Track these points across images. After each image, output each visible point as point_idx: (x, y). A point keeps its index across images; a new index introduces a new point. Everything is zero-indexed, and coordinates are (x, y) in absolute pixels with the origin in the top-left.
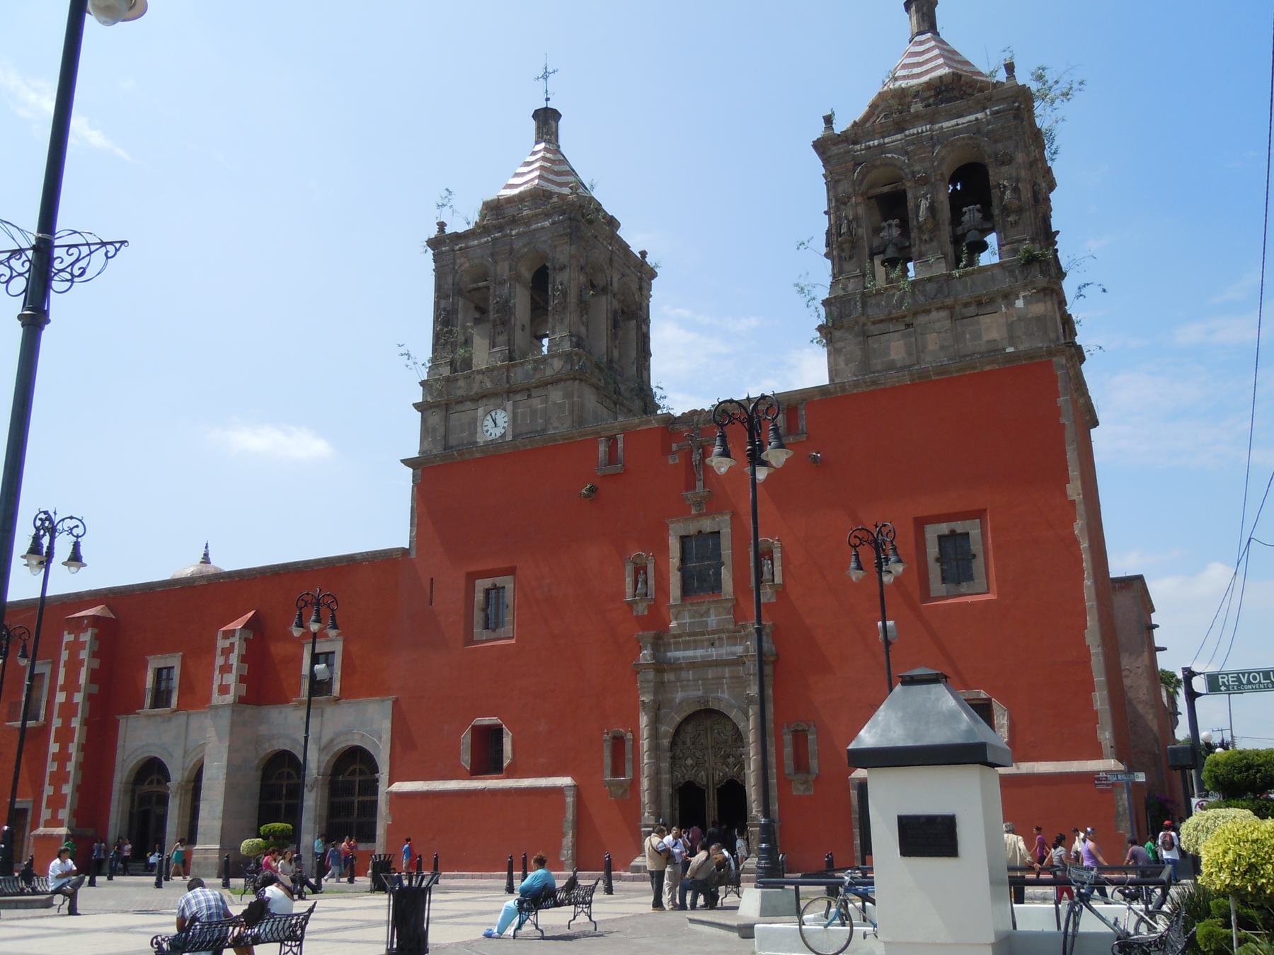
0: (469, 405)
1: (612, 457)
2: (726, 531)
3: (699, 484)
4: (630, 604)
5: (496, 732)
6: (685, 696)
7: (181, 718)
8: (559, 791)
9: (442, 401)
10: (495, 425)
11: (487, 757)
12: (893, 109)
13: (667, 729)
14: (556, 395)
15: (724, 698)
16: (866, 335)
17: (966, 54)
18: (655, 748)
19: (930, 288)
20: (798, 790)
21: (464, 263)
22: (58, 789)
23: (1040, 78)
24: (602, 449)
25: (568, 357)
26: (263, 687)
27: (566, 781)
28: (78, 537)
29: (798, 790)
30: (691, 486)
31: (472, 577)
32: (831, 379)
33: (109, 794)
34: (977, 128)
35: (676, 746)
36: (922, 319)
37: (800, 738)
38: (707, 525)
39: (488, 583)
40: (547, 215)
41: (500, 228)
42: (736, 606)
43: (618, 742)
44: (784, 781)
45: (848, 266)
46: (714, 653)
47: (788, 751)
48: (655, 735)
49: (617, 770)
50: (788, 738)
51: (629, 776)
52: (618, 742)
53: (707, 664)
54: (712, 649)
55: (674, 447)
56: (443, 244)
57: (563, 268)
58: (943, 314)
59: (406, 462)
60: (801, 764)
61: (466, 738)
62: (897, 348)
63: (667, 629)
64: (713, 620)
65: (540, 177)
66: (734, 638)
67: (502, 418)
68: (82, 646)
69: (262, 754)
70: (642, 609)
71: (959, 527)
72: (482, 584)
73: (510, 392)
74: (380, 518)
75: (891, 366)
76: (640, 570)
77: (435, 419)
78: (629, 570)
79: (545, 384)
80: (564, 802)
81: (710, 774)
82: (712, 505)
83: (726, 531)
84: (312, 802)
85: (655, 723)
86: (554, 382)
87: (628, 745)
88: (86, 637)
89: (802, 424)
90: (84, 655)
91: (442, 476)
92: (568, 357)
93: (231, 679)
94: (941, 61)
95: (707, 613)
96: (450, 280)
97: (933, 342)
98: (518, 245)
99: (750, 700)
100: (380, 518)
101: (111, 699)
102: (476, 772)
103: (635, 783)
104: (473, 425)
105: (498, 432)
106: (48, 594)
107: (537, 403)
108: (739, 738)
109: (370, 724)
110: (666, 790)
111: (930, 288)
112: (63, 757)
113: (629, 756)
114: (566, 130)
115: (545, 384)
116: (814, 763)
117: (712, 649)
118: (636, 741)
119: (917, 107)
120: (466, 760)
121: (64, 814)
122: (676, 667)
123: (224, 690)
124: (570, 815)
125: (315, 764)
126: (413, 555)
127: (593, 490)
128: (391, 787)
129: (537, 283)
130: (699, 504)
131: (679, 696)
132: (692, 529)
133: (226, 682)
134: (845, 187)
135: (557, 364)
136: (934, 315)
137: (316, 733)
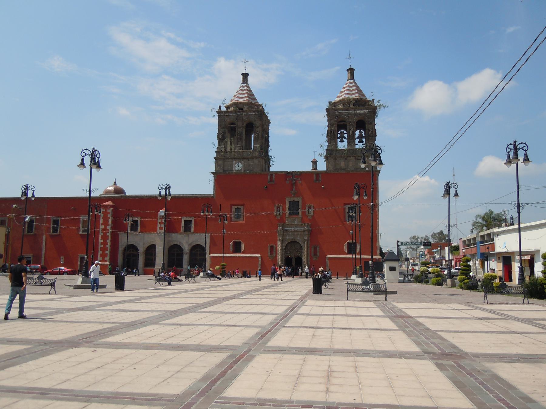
0: (230, 160)
1: (271, 180)
2: (300, 201)
3: (294, 189)
4: (276, 216)
5: (240, 243)
6: (289, 238)
7: (142, 234)
8: (257, 257)
9: (221, 158)
10: (238, 167)
11: (237, 248)
12: (345, 102)
13: (284, 245)
14: (256, 161)
15: (298, 239)
16: (336, 159)
17: (365, 92)
18: (282, 249)
19: (351, 151)
20: (314, 259)
21: (228, 120)
22: (104, 252)
23: (82, 164)
24: (269, 177)
25: (260, 152)
26: (171, 227)
27: (259, 255)
28: (526, 151)
29: (314, 259)
30: (292, 190)
31: (232, 205)
32: (327, 169)
33: (117, 254)
34: (364, 114)
35: (286, 249)
36: (349, 158)
37: (315, 248)
38: (296, 199)
39: (236, 207)
40: (254, 112)
41: (239, 112)
42: (302, 219)
43: (272, 247)
44: (311, 257)
45: (332, 141)
46: (296, 229)
47: (313, 251)
48: (282, 246)
49: (272, 253)
50: (313, 248)
51: (274, 255)
52: (272, 247)
53: (295, 231)
54: (296, 228)
55: (288, 179)
56: (219, 112)
57: (258, 127)
58: (354, 158)
59: (212, 173)
60: (315, 254)
61: (231, 244)
62: (342, 164)
63: (285, 223)
64: (296, 222)
65: (248, 97)
66: (301, 226)
67: (241, 165)
68: (109, 213)
69: (170, 245)
70: (279, 217)
71: (239, 207)
72: (234, 207)
73: (244, 158)
74: (205, 186)
75: (341, 168)
76: (278, 208)
77: (220, 162)
78: (275, 208)
79: (253, 158)
80: (258, 260)
81: (293, 255)
82: (297, 195)
83: (300, 201)
84: (186, 258)
85: (282, 243)
86: (256, 158)
87: (274, 248)
88: (110, 210)
89: (320, 179)
90: (110, 216)
91: (221, 177)
92: (260, 152)
93: (163, 226)
94: (356, 91)
95: (295, 220)
96: (224, 123)
97: (351, 164)
98: (244, 118)
99: (305, 240)
100: (205, 186)
101: (118, 227)
102: (234, 252)
103: (276, 257)
104: (232, 166)
105: (239, 169)
106: (92, 195)
107: (250, 163)
108: (301, 248)
109: (201, 239)
110: (284, 258)
111: (351, 151)
112: (105, 243)
113: (274, 250)
114: (250, 78)
115: (253, 158)
116: (318, 254)
117: (296, 228)
118: (276, 247)
119: (351, 105)
120: (231, 249)
121: (107, 259)
122: (287, 231)
123: (161, 228)
124: (260, 263)
125: (141, 249)
126: (215, 198)
127: (267, 187)
128: (209, 255)
129: (243, 126)
130: (294, 194)
131: (287, 238)
132: (292, 200)
133: (161, 227)
134: (333, 121)
135: (257, 153)
136: (352, 158)
137: (186, 241)
